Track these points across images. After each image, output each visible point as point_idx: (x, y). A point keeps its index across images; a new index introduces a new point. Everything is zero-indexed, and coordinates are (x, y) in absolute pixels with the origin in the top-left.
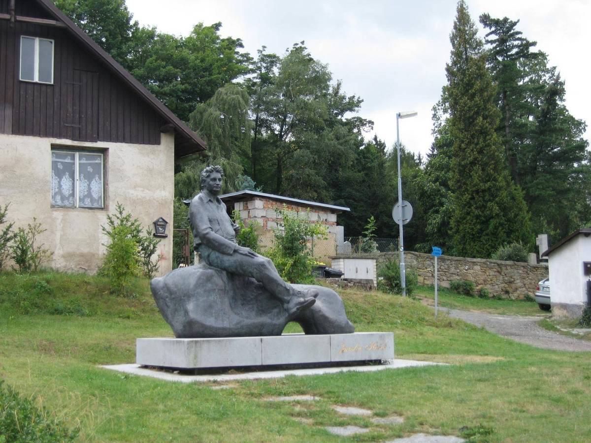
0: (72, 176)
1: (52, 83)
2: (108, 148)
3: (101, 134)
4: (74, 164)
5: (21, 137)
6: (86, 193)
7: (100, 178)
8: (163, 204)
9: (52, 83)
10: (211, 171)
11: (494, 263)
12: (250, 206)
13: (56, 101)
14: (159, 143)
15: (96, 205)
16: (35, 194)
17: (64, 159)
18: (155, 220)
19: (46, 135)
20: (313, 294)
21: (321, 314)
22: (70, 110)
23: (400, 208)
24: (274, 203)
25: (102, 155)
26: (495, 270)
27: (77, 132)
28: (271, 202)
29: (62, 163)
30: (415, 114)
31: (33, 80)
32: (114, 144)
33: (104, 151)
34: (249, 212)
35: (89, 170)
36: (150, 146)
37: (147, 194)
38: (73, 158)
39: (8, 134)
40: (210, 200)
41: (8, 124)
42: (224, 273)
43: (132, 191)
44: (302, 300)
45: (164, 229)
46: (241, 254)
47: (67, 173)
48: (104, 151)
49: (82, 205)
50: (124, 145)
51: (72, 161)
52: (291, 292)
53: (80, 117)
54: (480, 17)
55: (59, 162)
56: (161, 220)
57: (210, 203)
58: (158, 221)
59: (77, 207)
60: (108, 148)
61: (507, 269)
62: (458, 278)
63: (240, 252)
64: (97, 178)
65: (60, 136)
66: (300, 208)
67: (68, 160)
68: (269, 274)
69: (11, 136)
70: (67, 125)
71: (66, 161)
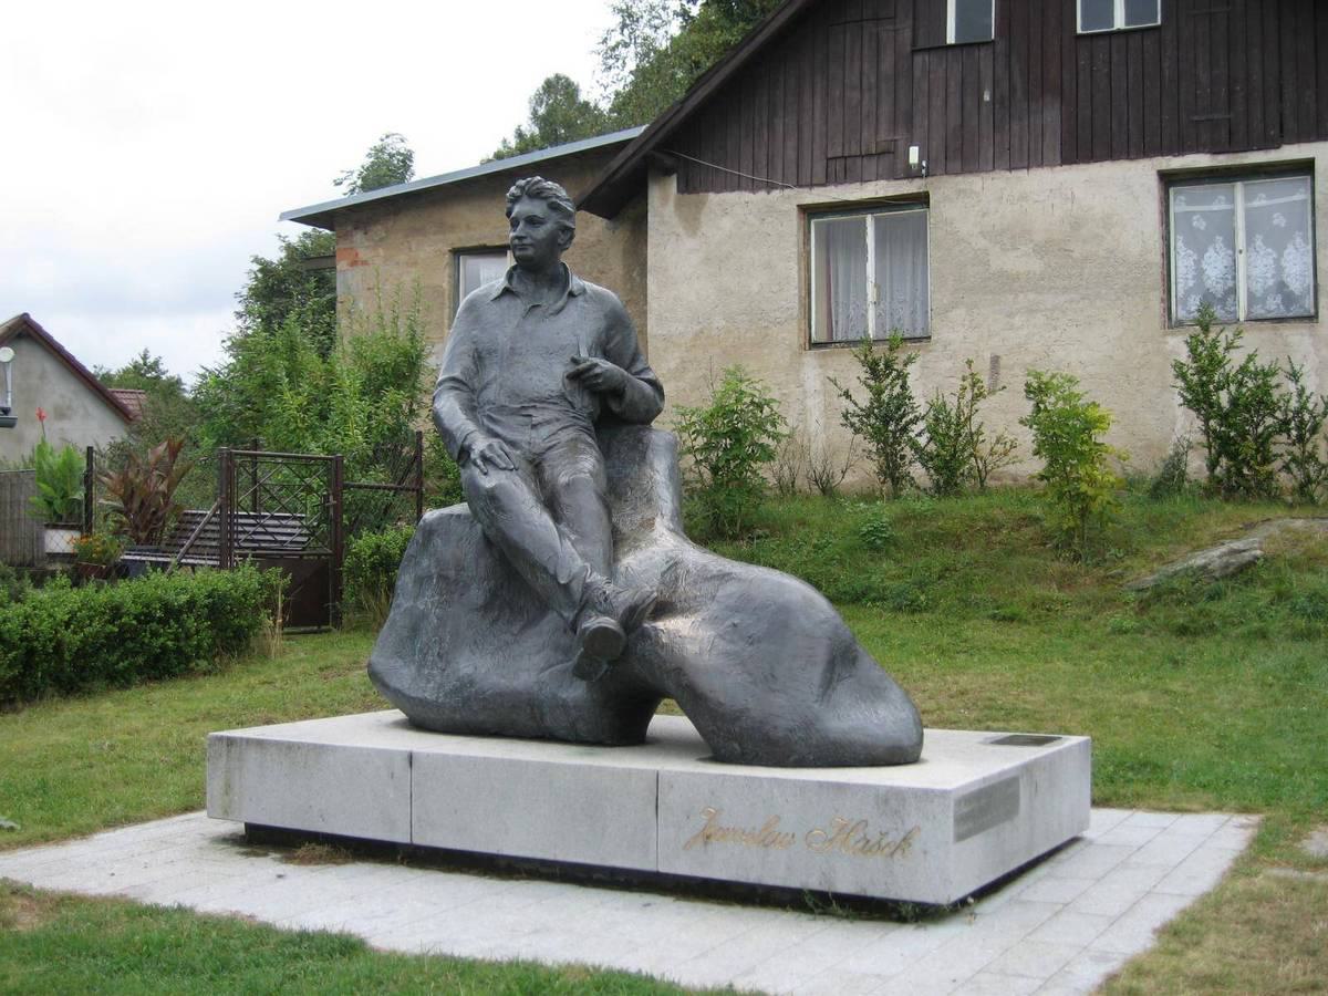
0: (1231, 243)
1: (1159, 22)
2: (1313, 159)
3: (1290, 124)
4: (1232, 213)
5: (1083, 167)
6: (1191, 283)
7: (1305, 239)
13: (1166, 64)
15: (1295, 311)
16: (1119, 298)
17: (1210, 204)
22: (1204, 77)
27: (1224, 132)
29: (1204, 214)
30: (1074, 841)
33: (1306, 167)
35: (1275, 222)
38: (1232, 200)
39: (1052, 165)
41: (1053, 142)
47: (1219, 238)
48: (1306, 167)
49: (1259, 311)
51: (1228, 207)
53: (1231, 93)
54: (1155, 931)
55: (1194, 213)
59: (1242, 319)
60: (1313, 159)
62: (888, 27)
64: (1298, 240)
65: (1180, 149)
67: (1219, 206)
69: (1059, 168)
70: (1196, 118)
71: (1215, 207)
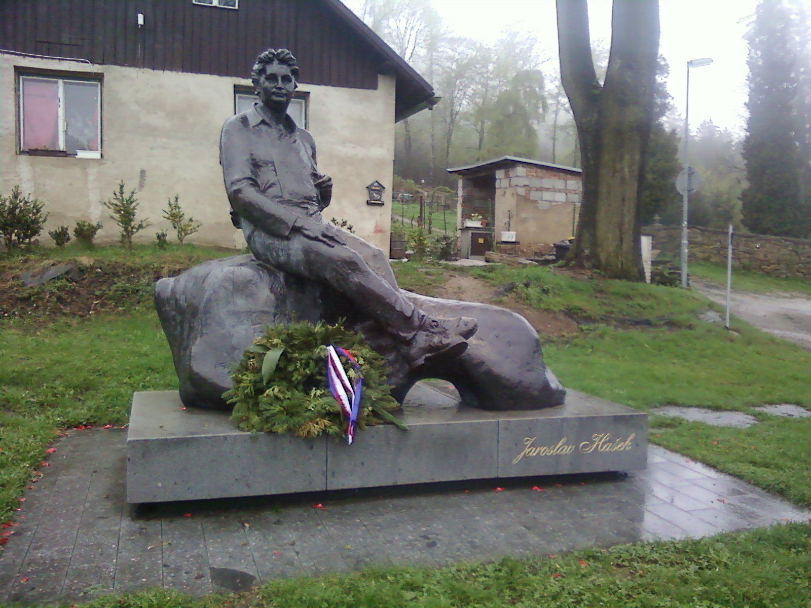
1: (237, 7)
2: (309, 93)
5: (194, 75)
8: (380, 163)
9: (237, 7)
10: (268, 61)
11: (790, 241)
12: (511, 174)
14: (374, 86)
18: (369, 183)
19: (227, 74)
20: (463, 328)
21: (483, 369)
23: (686, 176)
24: (539, 170)
25: (303, 101)
26: (791, 249)
28: (535, 169)
31: (212, 3)
32: (317, 87)
34: (510, 181)
36: (365, 90)
37: (360, 152)
40: (263, 122)
42: (281, 276)
43: (340, 148)
44: (436, 339)
45: (380, 195)
46: (308, 237)
50: (329, 88)
52: (416, 322)
56: (376, 184)
57: (263, 127)
58: (372, 185)
60: (309, 93)
61: (804, 248)
63: (306, 232)
66: (569, 176)
68: (370, 286)
69: (181, 73)
